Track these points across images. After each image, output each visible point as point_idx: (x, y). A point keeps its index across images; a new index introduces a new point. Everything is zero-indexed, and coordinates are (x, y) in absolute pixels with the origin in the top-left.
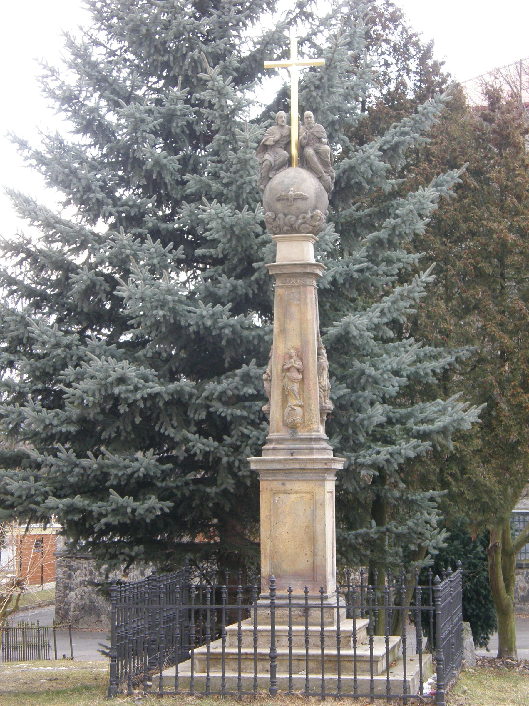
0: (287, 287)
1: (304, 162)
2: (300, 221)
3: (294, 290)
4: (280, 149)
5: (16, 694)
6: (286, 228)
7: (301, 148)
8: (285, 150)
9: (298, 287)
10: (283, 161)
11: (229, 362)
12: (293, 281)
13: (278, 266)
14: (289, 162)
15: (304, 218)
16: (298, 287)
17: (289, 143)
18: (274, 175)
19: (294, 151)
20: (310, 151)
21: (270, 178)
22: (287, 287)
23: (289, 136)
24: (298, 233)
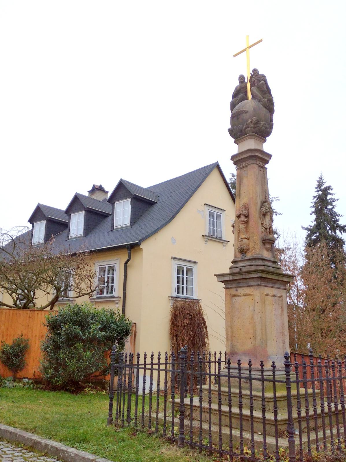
3: (244, 169)
12: (244, 163)
15: (247, 124)
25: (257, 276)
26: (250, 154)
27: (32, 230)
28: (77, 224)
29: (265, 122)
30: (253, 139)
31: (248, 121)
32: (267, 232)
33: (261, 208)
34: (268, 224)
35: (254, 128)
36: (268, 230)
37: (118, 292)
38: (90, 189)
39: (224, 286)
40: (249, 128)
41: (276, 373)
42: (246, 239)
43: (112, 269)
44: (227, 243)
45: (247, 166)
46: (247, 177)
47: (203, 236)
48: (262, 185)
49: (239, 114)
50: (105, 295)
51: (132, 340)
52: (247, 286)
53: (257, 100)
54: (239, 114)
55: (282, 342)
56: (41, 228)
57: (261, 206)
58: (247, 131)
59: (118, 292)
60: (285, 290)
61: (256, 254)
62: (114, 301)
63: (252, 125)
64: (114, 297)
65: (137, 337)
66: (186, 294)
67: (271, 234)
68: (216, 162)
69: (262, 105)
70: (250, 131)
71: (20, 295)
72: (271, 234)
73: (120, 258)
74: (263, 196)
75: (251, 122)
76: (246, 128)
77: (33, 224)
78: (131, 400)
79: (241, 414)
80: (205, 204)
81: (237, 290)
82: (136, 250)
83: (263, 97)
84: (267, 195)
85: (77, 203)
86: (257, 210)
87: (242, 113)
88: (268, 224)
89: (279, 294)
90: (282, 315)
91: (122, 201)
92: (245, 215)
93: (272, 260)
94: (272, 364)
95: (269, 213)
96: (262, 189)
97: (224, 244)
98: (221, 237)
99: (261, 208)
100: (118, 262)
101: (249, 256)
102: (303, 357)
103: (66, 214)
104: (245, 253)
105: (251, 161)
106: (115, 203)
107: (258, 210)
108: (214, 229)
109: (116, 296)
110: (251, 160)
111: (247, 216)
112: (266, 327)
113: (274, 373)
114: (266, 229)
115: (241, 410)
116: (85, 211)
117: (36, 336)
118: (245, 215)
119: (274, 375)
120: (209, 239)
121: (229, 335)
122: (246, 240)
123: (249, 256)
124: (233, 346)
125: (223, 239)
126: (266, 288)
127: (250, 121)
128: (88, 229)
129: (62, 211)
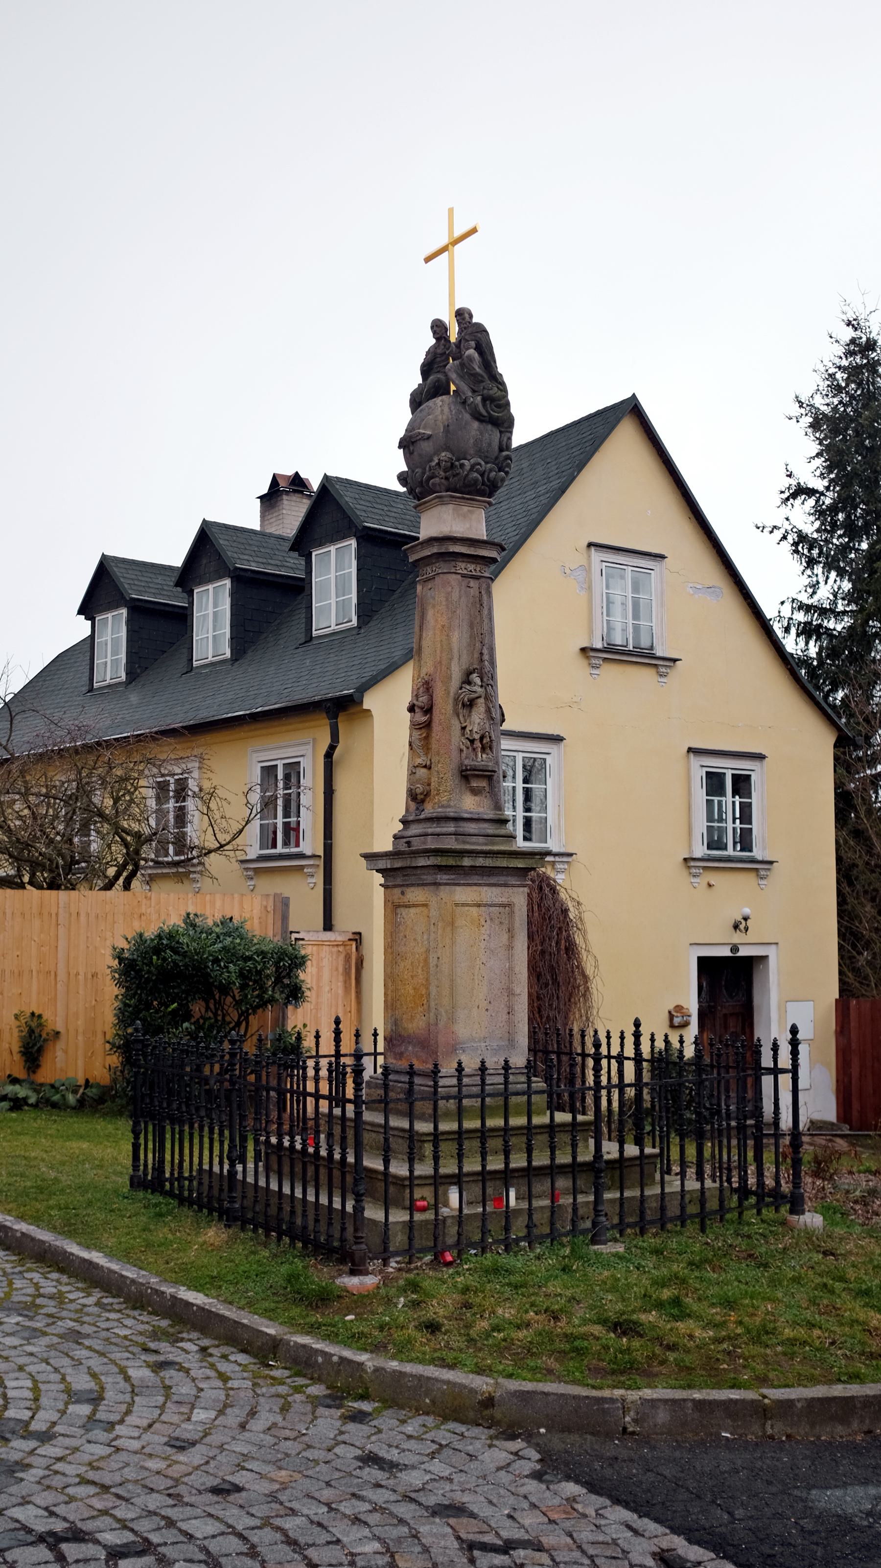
25: (429, 863)
26: (435, 550)
27: (92, 637)
28: (213, 614)
29: (480, 457)
32: (474, 749)
33: (461, 688)
34: (475, 730)
36: (478, 744)
37: (311, 842)
38: (265, 490)
39: (382, 881)
40: (437, 479)
41: (511, 1078)
42: (425, 767)
43: (293, 771)
44: (671, 664)
45: (433, 578)
47: (583, 650)
48: (471, 626)
49: (413, 443)
50: (280, 849)
51: (350, 978)
52: (418, 885)
55: (506, 1010)
56: (115, 626)
57: (463, 683)
59: (311, 842)
60: (522, 889)
61: (443, 806)
62: (302, 867)
64: (301, 856)
65: (365, 973)
66: (526, 839)
67: (488, 751)
68: (630, 395)
72: (488, 751)
73: (314, 740)
74: (473, 654)
75: (438, 464)
77: (90, 617)
79: (386, 1173)
80: (590, 545)
81: (403, 893)
82: (354, 714)
84: (485, 651)
85: (208, 543)
86: (449, 693)
88: (475, 730)
89: (504, 900)
90: (510, 947)
91: (332, 548)
92: (422, 708)
93: (491, 815)
94: (456, 1065)
95: (481, 701)
96: (472, 637)
97: (663, 670)
98: (652, 648)
99: (461, 688)
100: (308, 750)
101: (429, 810)
103: (179, 589)
104: (423, 801)
105: (443, 567)
106: (314, 554)
107: (452, 694)
108: (634, 619)
109: (309, 853)
110: (442, 564)
111: (428, 710)
112: (452, 980)
113: (460, 1080)
114: (472, 741)
115: (386, 1163)
116: (232, 578)
117: (77, 974)
118: (422, 708)
119: (506, 1083)
120: (605, 659)
121: (389, 998)
122: (424, 770)
123: (429, 810)
124: (396, 1023)
125: (659, 653)
126: (458, 888)
128: (247, 634)
129: (170, 568)
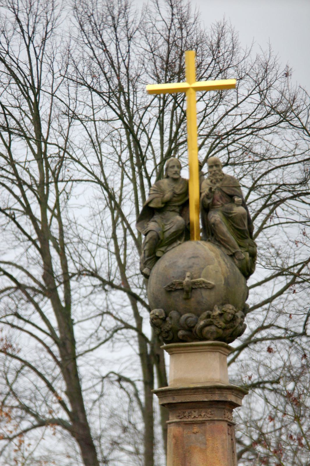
0: (186, 424)
1: (210, 232)
2: (202, 323)
3: (196, 429)
4: (172, 214)
5: (82, 181)
6: (181, 333)
7: (205, 209)
8: (181, 214)
9: (203, 423)
10: (175, 232)
11: (35, 131)
12: (195, 414)
13: (169, 390)
14: (185, 233)
15: (209, 316)
16: (203, 423)
17: (186, 204)
18: (164, 253)
19: (194, 216)
20: (216, 217)
21: (158, 258)
22: (186, 424)
23: (186, 193)
24: (201, 340)
30: (218, 354)
31: (212, 310)
35: (224, 329)
40: (213, 328)
46: (203, 451)
53: (226, 252)
54: (192, 289)
58: (208, 332)
63: (222, 324)
69: (240, 269)
70: (212, 333)
71: (222, 57)
75: (221, 315)
76: (206, 326)
78: (65, 379)
83: (240, 246)
87: (200, 288)
102: (50, 71)
127: (217, 312)
